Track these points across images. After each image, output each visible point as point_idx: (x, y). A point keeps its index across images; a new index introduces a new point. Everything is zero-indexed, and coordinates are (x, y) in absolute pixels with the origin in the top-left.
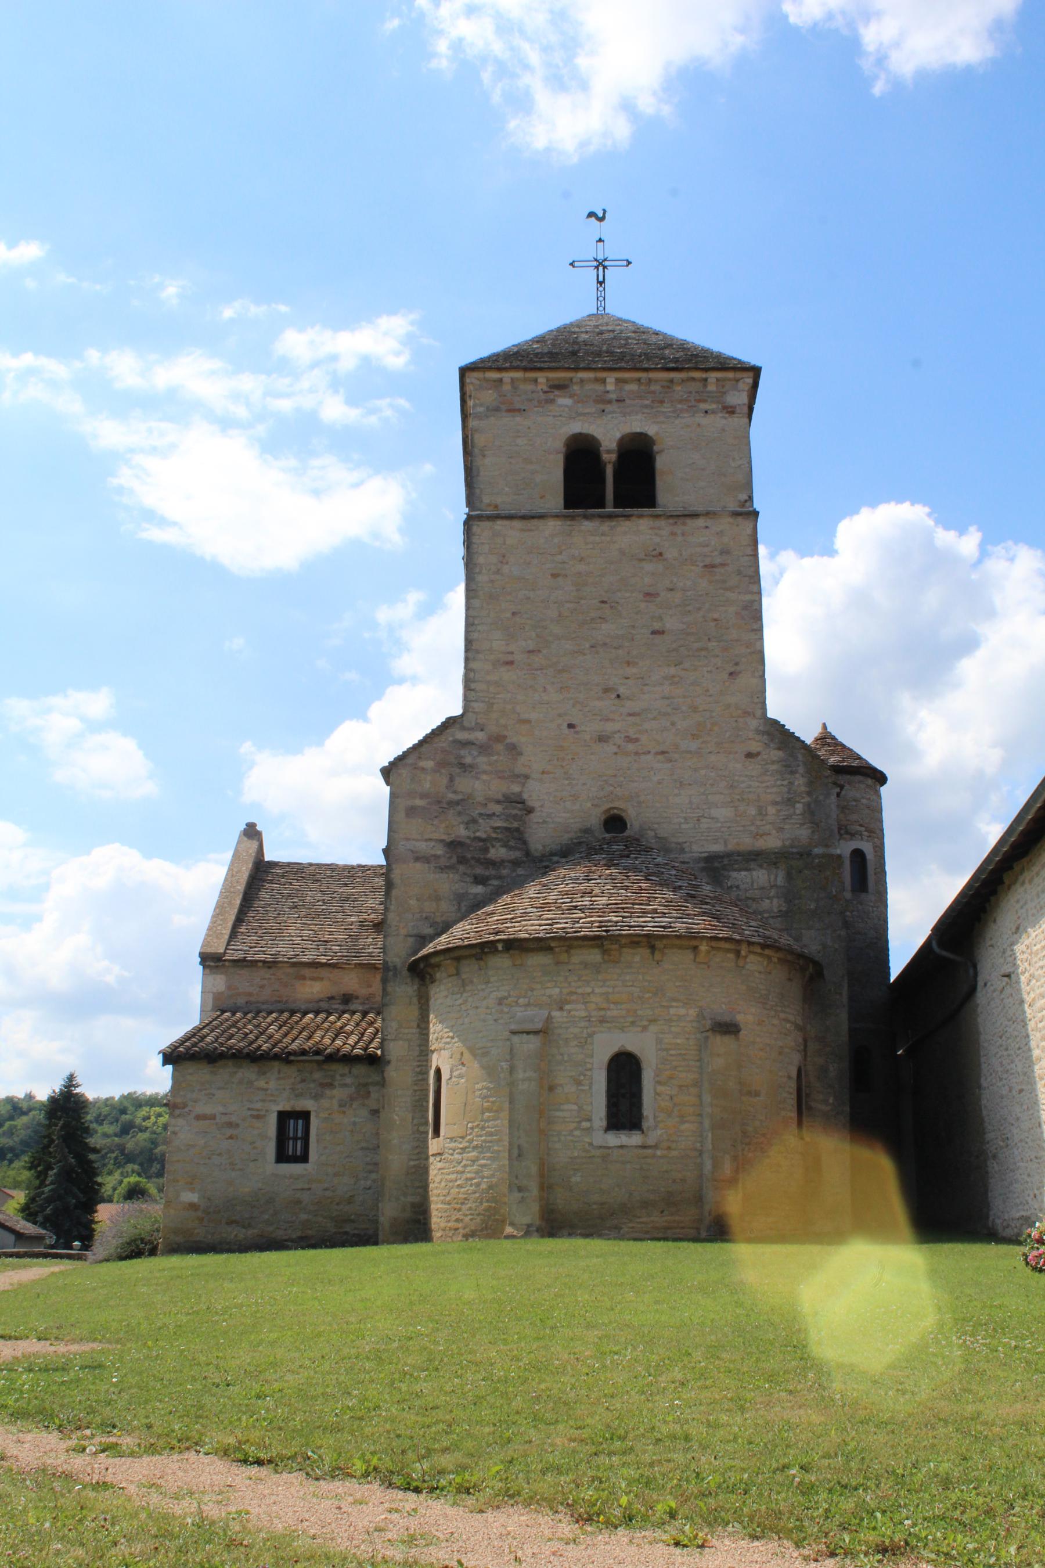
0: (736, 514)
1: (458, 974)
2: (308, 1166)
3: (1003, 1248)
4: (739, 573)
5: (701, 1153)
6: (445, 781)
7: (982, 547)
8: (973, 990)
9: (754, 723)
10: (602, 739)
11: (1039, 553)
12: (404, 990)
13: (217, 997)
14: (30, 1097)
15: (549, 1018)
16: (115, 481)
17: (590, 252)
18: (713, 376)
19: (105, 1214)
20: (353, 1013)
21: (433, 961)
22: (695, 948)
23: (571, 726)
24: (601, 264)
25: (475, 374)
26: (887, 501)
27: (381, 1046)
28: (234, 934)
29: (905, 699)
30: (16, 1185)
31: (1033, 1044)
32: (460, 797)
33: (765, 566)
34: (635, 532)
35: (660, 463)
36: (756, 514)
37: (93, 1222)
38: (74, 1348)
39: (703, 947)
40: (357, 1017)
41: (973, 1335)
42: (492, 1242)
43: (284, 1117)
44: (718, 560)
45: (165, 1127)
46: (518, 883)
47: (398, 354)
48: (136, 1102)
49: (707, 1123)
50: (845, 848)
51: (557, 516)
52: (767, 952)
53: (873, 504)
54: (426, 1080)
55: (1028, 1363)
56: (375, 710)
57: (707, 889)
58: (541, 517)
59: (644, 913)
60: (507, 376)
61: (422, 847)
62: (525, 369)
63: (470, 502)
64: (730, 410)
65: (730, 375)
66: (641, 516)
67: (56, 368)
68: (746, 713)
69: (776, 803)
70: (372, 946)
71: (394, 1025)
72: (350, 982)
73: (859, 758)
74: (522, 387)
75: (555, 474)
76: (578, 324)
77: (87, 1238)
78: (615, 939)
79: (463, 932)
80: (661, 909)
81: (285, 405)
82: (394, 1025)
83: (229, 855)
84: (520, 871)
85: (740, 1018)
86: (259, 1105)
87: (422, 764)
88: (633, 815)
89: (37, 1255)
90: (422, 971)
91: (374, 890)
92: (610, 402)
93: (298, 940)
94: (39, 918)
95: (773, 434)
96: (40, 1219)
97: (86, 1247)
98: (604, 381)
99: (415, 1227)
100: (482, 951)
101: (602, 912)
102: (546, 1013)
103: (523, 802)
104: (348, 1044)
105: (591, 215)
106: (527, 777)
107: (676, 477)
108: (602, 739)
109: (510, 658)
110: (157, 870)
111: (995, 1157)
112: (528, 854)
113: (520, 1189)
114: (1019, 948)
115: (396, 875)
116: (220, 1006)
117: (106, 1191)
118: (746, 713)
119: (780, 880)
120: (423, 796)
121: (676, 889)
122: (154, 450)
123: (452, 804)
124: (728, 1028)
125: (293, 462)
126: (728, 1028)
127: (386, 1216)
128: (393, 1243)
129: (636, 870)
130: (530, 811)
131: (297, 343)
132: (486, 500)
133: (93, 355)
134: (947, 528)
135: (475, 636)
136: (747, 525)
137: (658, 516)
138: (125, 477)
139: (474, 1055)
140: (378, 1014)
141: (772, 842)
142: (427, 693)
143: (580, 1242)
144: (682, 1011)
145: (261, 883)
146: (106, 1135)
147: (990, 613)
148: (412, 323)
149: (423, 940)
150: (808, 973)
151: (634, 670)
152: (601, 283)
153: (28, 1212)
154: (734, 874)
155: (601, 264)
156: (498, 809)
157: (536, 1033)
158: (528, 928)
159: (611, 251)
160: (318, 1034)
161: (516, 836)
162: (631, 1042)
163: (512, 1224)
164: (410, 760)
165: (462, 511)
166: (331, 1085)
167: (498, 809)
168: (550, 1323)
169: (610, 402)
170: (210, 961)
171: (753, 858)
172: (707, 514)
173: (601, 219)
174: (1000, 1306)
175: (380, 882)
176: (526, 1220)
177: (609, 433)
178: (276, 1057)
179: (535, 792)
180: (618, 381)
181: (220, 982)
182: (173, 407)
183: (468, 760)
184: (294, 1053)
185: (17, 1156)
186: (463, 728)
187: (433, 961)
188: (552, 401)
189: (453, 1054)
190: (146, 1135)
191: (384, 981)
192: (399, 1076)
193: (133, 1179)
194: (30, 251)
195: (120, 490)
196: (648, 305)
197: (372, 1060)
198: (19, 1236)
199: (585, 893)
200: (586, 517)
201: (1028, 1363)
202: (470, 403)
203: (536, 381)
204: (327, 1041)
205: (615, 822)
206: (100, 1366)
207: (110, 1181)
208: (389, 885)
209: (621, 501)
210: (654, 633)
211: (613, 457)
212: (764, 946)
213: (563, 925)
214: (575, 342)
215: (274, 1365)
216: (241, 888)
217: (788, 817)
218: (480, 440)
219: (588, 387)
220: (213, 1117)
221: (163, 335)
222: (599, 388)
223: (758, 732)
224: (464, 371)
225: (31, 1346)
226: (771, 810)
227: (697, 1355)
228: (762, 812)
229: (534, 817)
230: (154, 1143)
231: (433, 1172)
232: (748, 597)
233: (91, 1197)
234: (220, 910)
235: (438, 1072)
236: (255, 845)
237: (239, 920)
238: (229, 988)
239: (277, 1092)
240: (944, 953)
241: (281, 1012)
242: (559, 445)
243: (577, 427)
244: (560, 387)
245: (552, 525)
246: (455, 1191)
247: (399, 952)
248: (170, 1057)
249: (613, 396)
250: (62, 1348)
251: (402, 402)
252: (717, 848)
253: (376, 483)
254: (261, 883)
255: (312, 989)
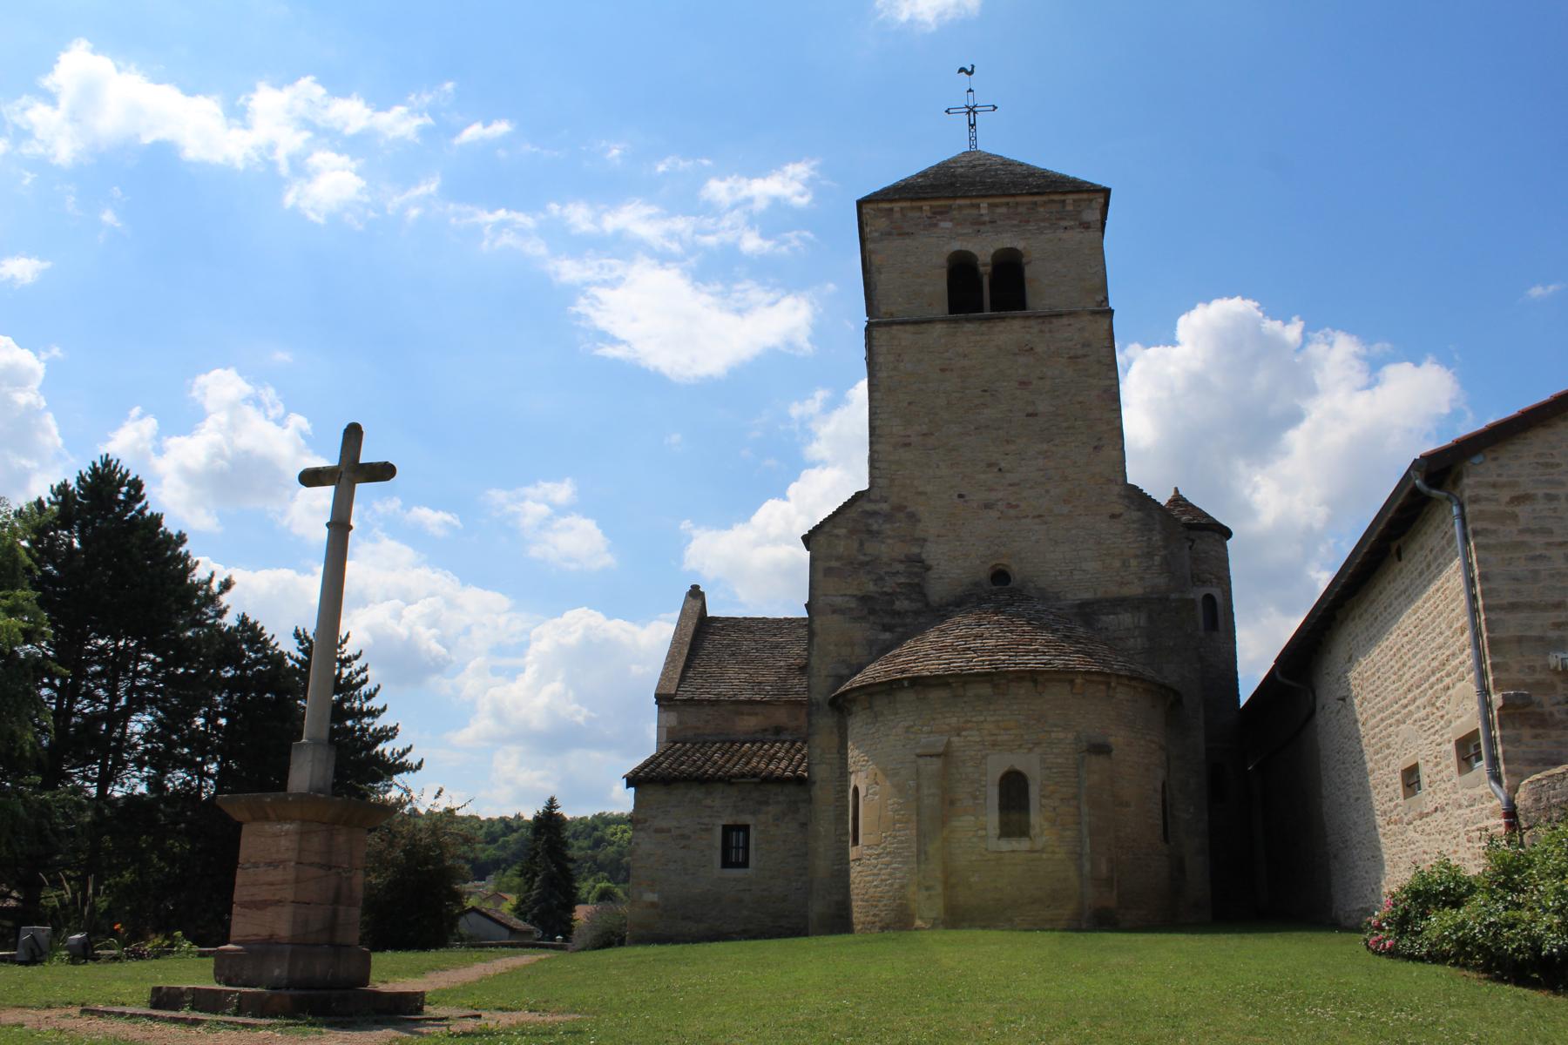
0: (1094, 313)
1: (871, 707)
2: (749, 871)
3: (1345, 936)
4: (1099, 362)
5: (1081, 855)
6: (856, 545)
7: (1304, 333)
8: (1312, 712)
9: (1117, 489)
10: (988, 506)
11: (1354, 338)
12: (825, 722)
13: (670, 731)
14: (519, 817)
15: (949, 743)
16: (574, 310)
17: (962, 100)
18: (1070, 198)
19: (581, 913)
20: (783, 742)
21: (850, 696)
22: (1072, 682)
23: (961, 496)
24: (971, 110)
25: (874, 206)
26: (1220, 297)
27: (807, 769)
28: (683, 678)
29: (1241, 466)
30: (510, 890)
31: (1367, 758)
32: (867, 559)
33: (1120, 358)
34: (1009, 332)
35: (1028, 272)
36: (1112, 312)
37: (572, 920)
38: (559, 1018)
39: (1079, 681)
40: (787, 745)
41: (1323, 1007)
42: (904, 933)
43: (727, 830)
44: (1080, 352)
45: (630, 842)
46: (918, 631)
47: (802, 195)
48: (604, 821)
49: (1085, 831)
50: (1198, 594)
51: (942, 321)
52: (1133, 683)
53: (1208, 301)
54: (846, 797)
55: (1374, 1031)
56: (793, 489)
57: (1081, 631)
58: (930, 321)
59: (1028, 652)
60: (897, 206)
61: (839, 600)
62: (912, 200)
63: (870, 310)
64: (1086, 226)
65: (1085, 196)
66: (1014, 318)
67: (524, 220)
68: (1109, 481)
69: (1136, 556)
70: (797, 685)
71: (818, 751)
72: (781, 716)
73: (1207, 516)
74: (910, 214)
75: (941, 285)
76: (954, 160)
77: (567, 930)
78: (1004, 674)
79: (874, 672)
80: (1041, 648)
81: (711, 240)
82: (818, 751)
83: (677, 614)
84: (922, 620)
85: (1112, 740)
86: (706, 820)
87: (836, 531)
88: (1014, 568)
89: (527, 946)
90: (841, 705)
91: (799, 639)
92: (984, 223)
93: (736, 682)
94: (522, 670)
95: (1122, 244)
96: (529, 917)
97: (566, 939)
98: (978, 206)
99: (839, 921)
100: (891, 687)
101: (992, 652)
102: (945, 739)
103: (922, 561)
104: (781, 767)
105: (962, 70)
106: (925, 540)
107: (1045, 283)
108: (988, 506)
109: (907, 440)
110: (617, 628)
111: (1335, 857)
112: (927, 604)
113: (928, 889)
114: (1352, 675)
115: (817, 625)
116: (671, 739)
117: (583, 893)
118: (1109, 481)
119: (1143, 623)
120: (838, 558)
121: (1054, 631)
122: (605, 284)
123: (863, 564)
124: (1101, 749)
125: (719, 288)
126: (1101, 749)
127: (810, 909)
128: (820, 934)
129: (1019, 616)
130: (928, 568)
131: (718, 189)
132: (883, 309)
133: (554, 208)
134: (1272, 319)
135: (878, 423)
136: (1104, 323)
137: (1028, 317)
138: (582, 306)
139: (887, 776)
140: (805, 742)
141: (1135, 590)
142: (836, 473)
143: (979, 932)
144: (1062, 735)
145: (704, 635)
146: (580, 848)
147: (1312, 391)
148: (813, 169)
149: (842, 679)
150: (1170, 701)
151: (1013, 447)
152: (972, 126)
153: (519, 911)
154: (1104, 618)
155: (971, 110)
156: (901, 567)
157: (938, 755)
158: (931, 666)
159: (980, 99)
160: (755, 760)
161: (917, 589)
162: (1019, 761)
163: (921, 918)
164: (827, 529)
165: (863, 319)
166: (767, 803)
167: (901, 567)
168: (955, 998)
169: (984, 223)
170: (663, 700)
171: (1118, 604)
172: (1070, 314)
173: (970, 73)
174: (1346, 984)
175: (803, 632)
176: (933, 914)
177: (984, 248)
178: (720, 780)
179: (934, 553)
180: (990, 205)
181: (672, 719)
182: (623, 247)
183: (875, 527)
184: (735, 776)
185: (509, 866)
186: (870, 501)
187: (850, 696)
188: (936, 225)
189: (869, 776)
190: (614, 848)
191: (809, 715)
192: (823, 793)
193: (604, 885)
194: (501, 128)
195: (579, 316)
196: (1013, 140)
197: (800, 781)
198: (513, 931)
199: (976, 637)
200: (968, 320)
201: (1374, 1031)
202: (867, 230)
203: (920, 209)
204: (762, 765)
205: (1000, 576)
206: (580, 1032)
207: (585, 887)
208: (812, 634)
209: (996, 306)
210: (1028, 415)
211: (989, 269)
212: (1131, 678)
213: (958, 664)
214: (953, 175)
215: (723, 1031)
216: (688, 639)
217: (1148, 568)
218: (876, 260)
219: (965, 212)
220: (669, 831)
221: (609, 189)
222: (975, 212)
223: (1119, 495)
224: (861, 204)
225: (524, 1016)
226: (1133, 562)
227: (1083, 1024)
228: (1125, 564)
229: (932, 574)
230: (621, 854)
231: (853, 875)
232: (1108, 382)
233: (571, 901)
234: (671, 658)
235: (856, 790)
236: (699, 604)
237: (687, 666)
238: (680, 723)
239: (721, 810)
240: (1287, 682)
241: (724, 742)
242: (943, 261)
243: (957, 246)
244: (936, 212)
245: (939, 328)
246: (872, 890)
247: (822, 690)
248: (633, 780)
249: (987, 219)
250: (549, 1019)
251: (807, 234)
252: (1087, 596)
253: (788, 302)
254: (704, 635)
255: (749, 723)
